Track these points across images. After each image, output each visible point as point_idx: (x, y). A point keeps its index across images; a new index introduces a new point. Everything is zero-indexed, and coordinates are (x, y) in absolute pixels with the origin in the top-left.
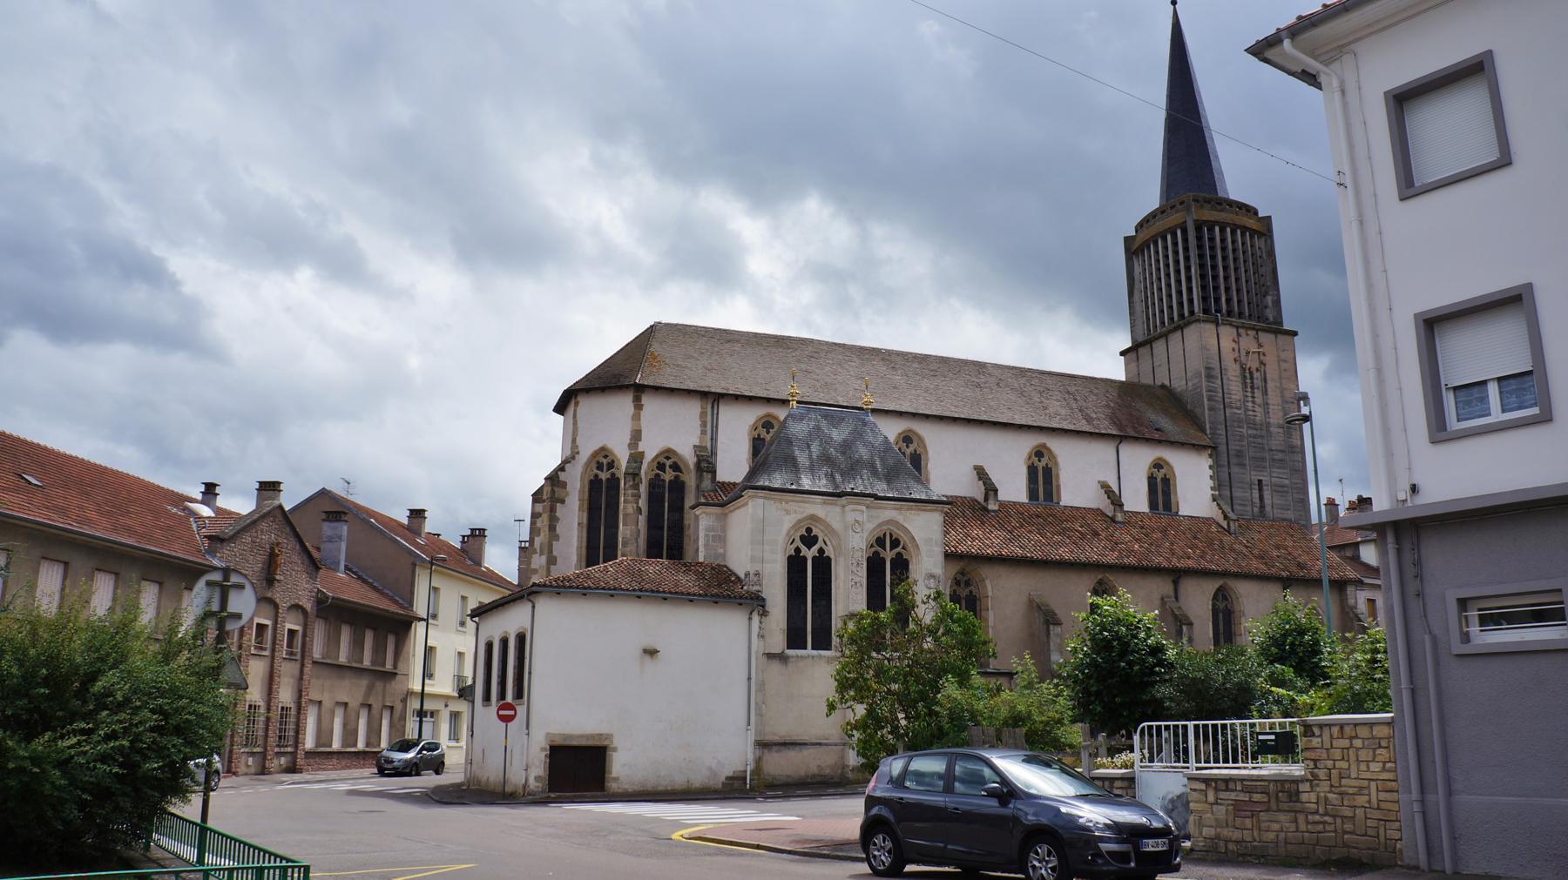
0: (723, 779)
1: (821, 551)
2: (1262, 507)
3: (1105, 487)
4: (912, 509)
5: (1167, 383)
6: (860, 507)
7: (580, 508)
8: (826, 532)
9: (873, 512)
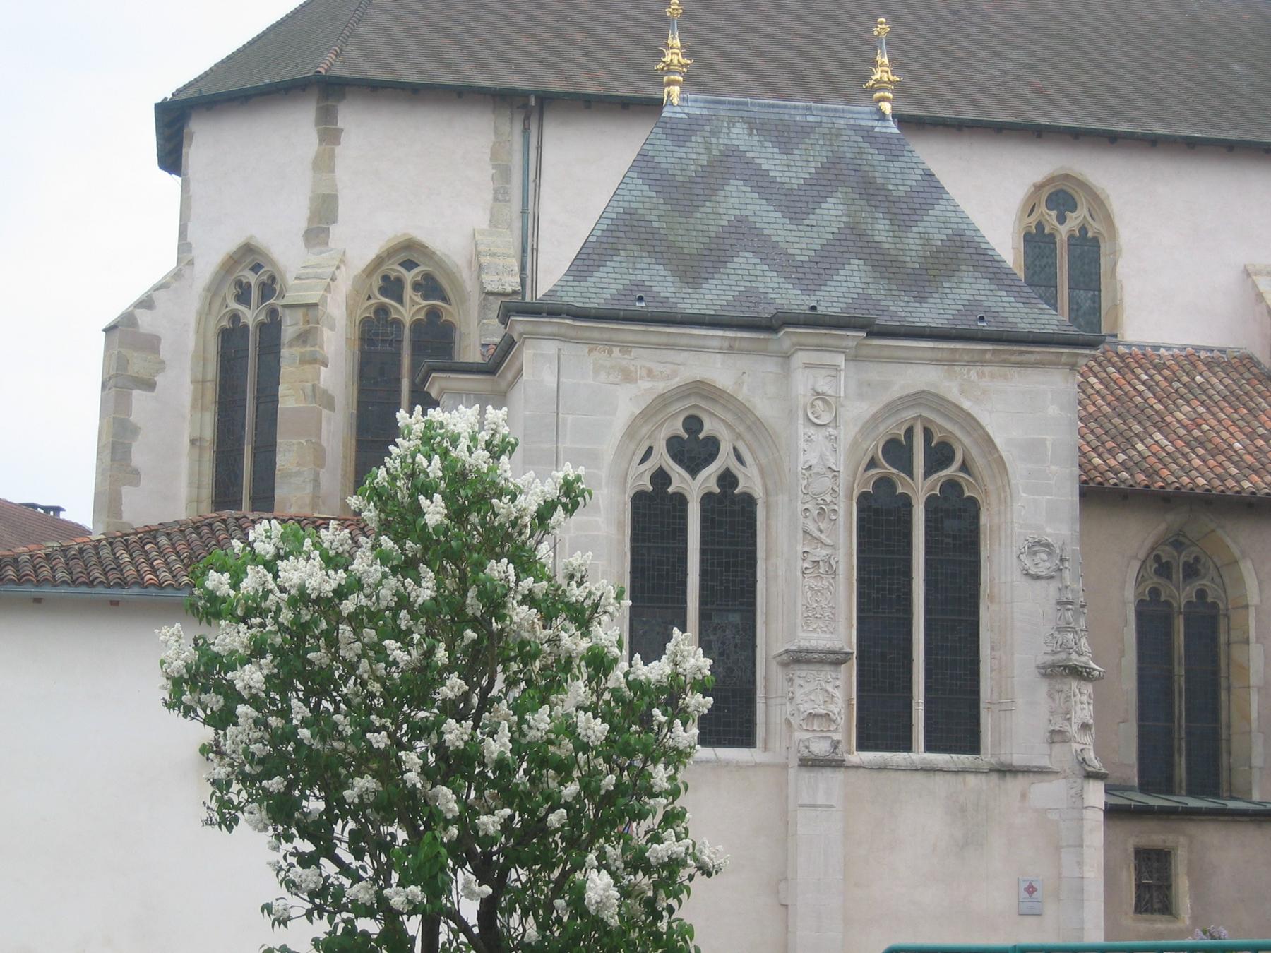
1: (728, 479)
4: (983, 363)
6: (827, 358)
7: (195, 400)
8: (741, 429)
9: (874, 373)
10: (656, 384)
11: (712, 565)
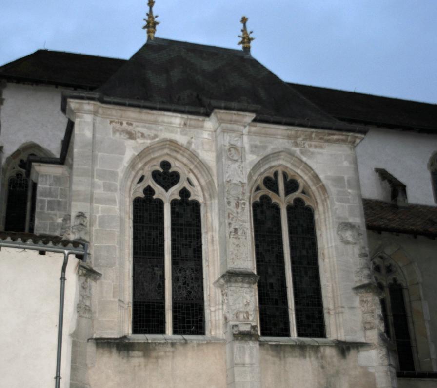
1: (184, 193)
10: (146, 141)
11: (178, 236)
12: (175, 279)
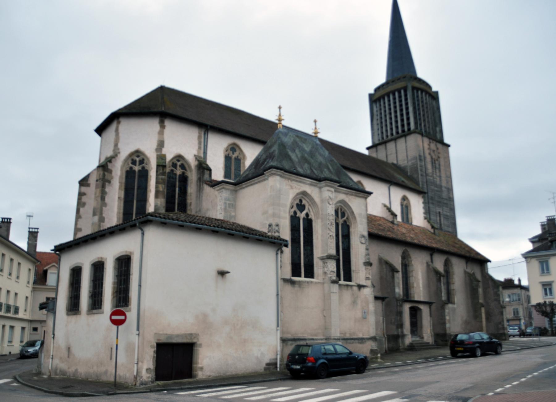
0: (264, 365)
1: (307, 215)
2: (441, 225)
3: (385, 206)
5: (395, 162)
12: (304, 254)
